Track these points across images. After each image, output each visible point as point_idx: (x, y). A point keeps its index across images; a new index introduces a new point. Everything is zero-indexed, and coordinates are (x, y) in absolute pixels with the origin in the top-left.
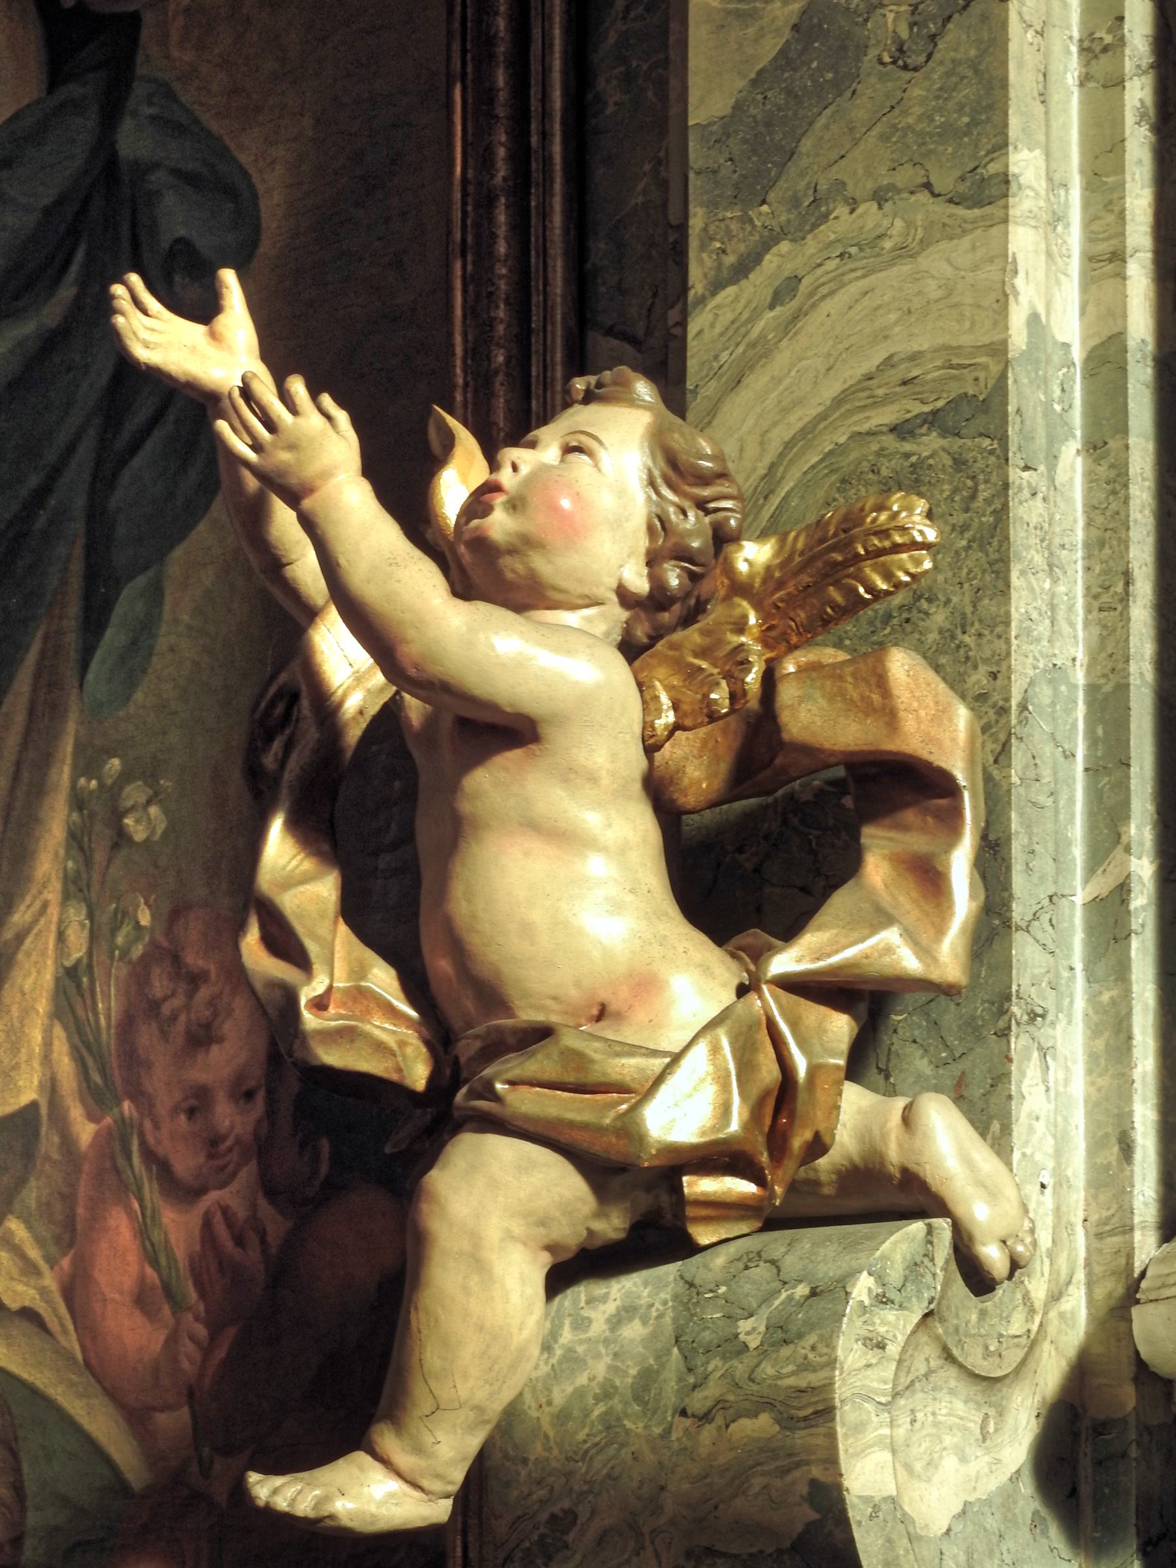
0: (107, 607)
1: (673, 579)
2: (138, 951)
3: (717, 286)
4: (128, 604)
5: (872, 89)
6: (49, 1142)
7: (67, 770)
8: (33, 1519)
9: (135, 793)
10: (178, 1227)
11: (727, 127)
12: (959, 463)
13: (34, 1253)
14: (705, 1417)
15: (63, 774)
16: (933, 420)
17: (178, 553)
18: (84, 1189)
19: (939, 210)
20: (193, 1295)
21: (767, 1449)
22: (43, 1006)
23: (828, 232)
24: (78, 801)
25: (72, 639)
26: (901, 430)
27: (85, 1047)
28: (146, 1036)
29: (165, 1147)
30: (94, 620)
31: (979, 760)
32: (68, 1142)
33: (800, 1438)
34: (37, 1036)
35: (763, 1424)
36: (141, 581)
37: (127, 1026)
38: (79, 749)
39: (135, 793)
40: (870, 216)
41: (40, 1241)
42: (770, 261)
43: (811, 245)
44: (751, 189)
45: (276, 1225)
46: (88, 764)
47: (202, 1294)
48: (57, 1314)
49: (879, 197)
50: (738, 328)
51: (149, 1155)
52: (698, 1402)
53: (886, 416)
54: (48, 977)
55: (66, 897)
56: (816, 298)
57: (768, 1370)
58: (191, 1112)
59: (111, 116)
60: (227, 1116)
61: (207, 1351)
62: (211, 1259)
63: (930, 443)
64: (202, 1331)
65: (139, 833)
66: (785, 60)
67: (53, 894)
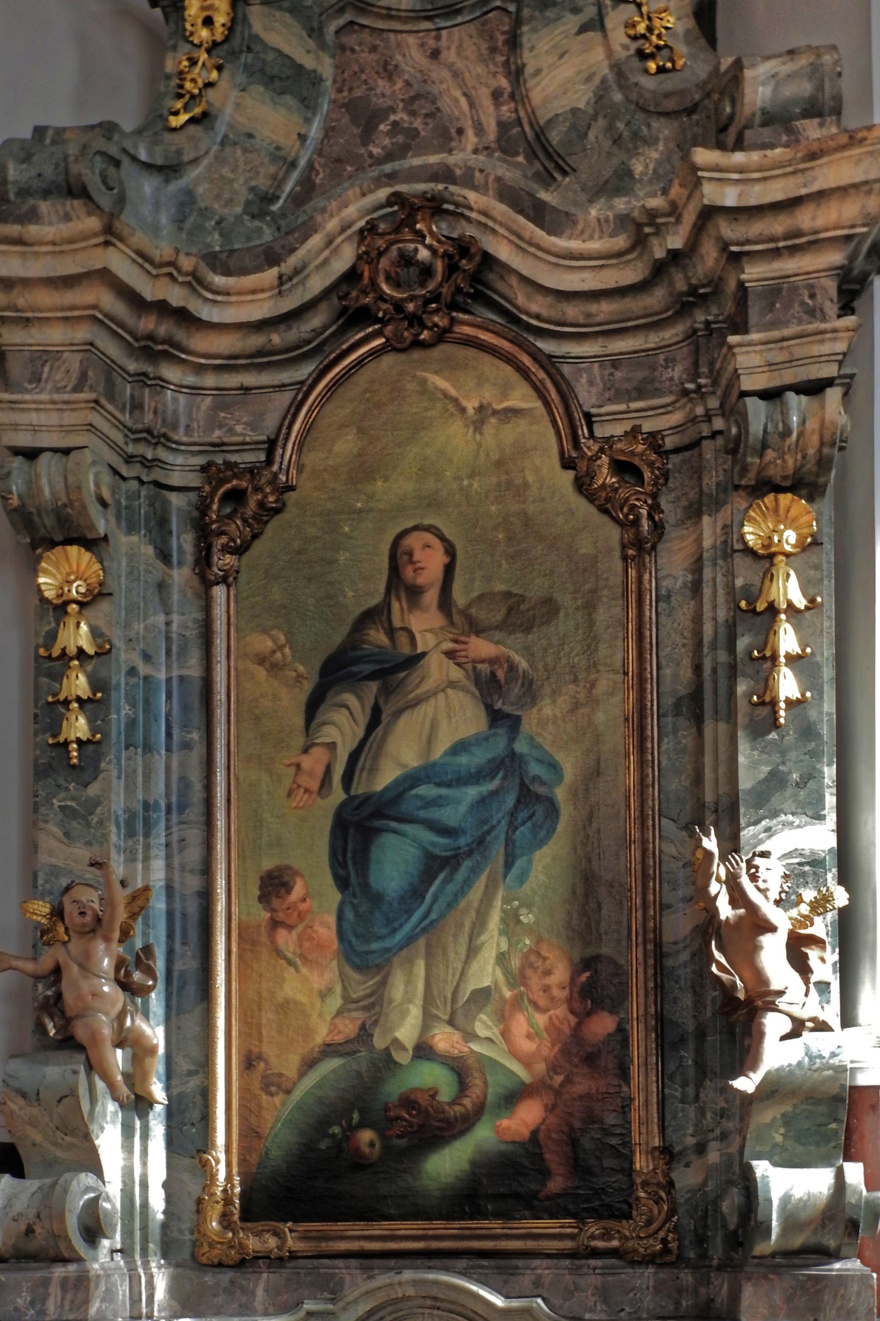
0: (513, 863)
1: (783, 896)
2: (525, 950)
3: (749, 825)
4: (519, 863)
5: (789, 792)
6: (495, 995)
7: (499, 903)
8: (490, 1090)
9: (523, 911)
10: (541, 1020)
11: (750, 792)
12: (814, 873)
13: (490, 1023)
14: (816, 1071)
15: (498, 903)
16: (808, 863)
17: (538, 853)
18: (507, 1008)
19: (808, 819)
20: (546, 1036)
21: (829, 1078)
22: (492, 961)
23: (779, 819)
24: (504, 911)
25: (501, 870)
26: (799, 864)
27: (507, 972)
28: (529, 972)
29: (535, 997)
30: (508, 865)
31: (451, 888)
32: (502, 997)
33: (839, 1075)
34: (490, 969)
35: (830, 1072)
36: (525, 858)
37: (522, 968)
38: (503, 897)
39: (523, 911)
40: (790, 818)
41: (492, 1021)
42: (763, 823)
43: (775, 821)
44: (758, 806)
45: (573, 1020)
46: (507, 900)
47: (549, 1035)
48: (498, 1039)
49: (793, 814)
50: (755, 836)
51: (530, 1001)
52: (814, 1067)
53: (797, 860)
54: (494, 954)
55: (500, 934)
56: (775, 833)
57: (831, 1061)
58: (544, 991)
59: (512, 740)
60: (556, 992)
61: (551, 1049)
62: (552, 1027)
63: (807, 868)
64: (549, 1045)
65: (525, 921)
66: (766, 779)
67: (496, 933)
